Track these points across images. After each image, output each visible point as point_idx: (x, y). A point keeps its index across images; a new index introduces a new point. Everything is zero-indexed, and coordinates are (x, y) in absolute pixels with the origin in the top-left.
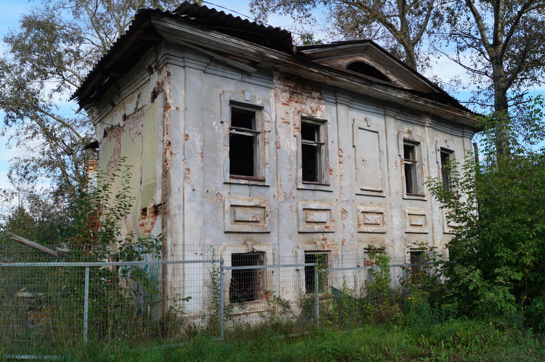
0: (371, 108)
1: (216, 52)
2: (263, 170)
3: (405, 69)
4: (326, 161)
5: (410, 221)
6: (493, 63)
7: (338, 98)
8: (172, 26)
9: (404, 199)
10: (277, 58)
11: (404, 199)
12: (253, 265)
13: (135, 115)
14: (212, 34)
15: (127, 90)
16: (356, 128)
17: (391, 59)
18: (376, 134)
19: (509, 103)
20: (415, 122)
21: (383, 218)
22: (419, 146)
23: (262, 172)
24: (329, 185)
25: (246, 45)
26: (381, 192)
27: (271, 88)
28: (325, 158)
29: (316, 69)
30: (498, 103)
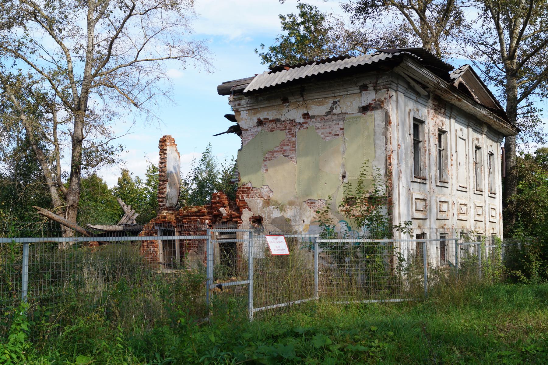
0: (463, 120)
1: (418, 82)
2: (424, 172)
3: (484, 89)
4: (445, 164)
5: (477, 212)
6: (508, 74)
7: (453, 113)
8: (410, 65)
9: (474, 194)
10: (444, 87)
11: (474, 194)
12: (171, 235)
13: (326, 118)
14: (424, 70)
15: (319, 94)
16: (458, 137)
17: (478, 81)
18: (464, 141)
19: (517, 111)
20: (479, 131)
21: (467, 209)
22: (480, 150)
23: (423, 172)
24: (448, 183)
25: (434, 77)
26: (466, 188)
27: (426, 106)
28: (444, 161)
29: (456, 94)
30: (510, 110)
